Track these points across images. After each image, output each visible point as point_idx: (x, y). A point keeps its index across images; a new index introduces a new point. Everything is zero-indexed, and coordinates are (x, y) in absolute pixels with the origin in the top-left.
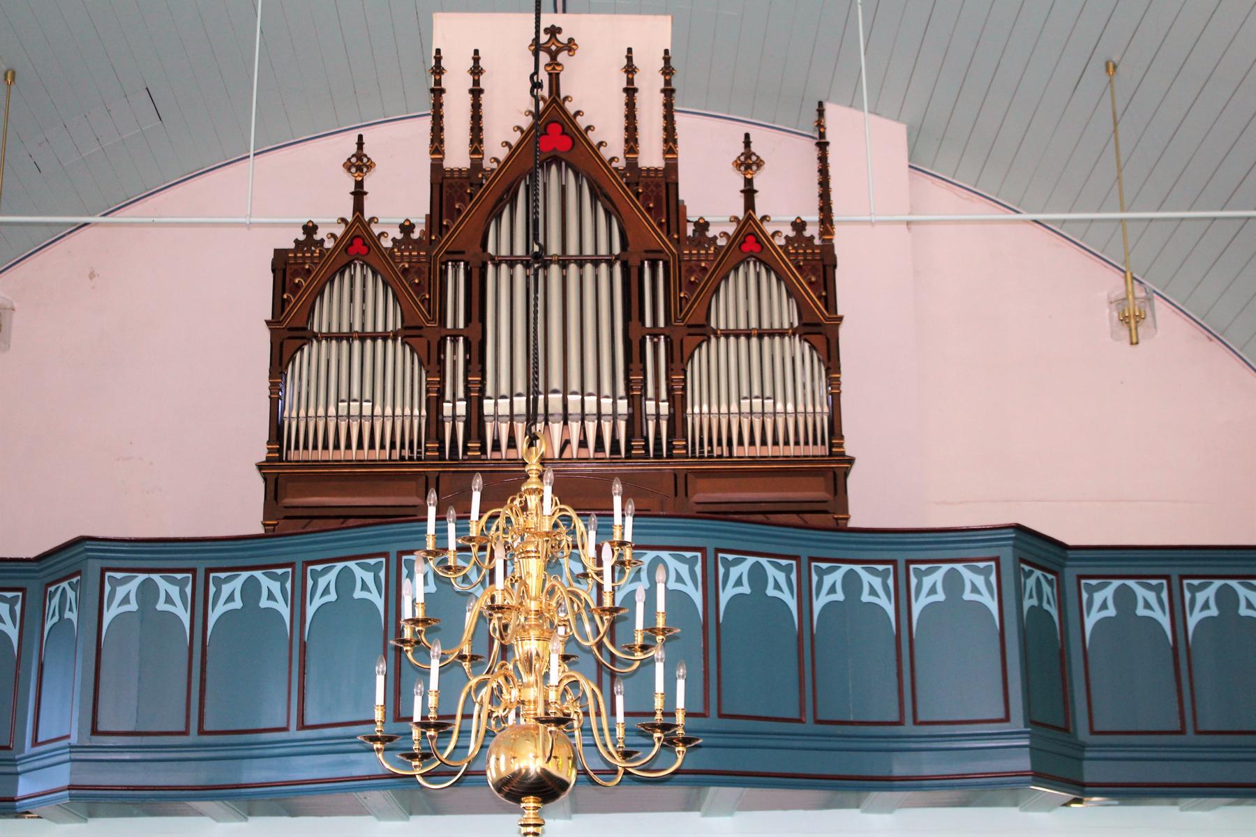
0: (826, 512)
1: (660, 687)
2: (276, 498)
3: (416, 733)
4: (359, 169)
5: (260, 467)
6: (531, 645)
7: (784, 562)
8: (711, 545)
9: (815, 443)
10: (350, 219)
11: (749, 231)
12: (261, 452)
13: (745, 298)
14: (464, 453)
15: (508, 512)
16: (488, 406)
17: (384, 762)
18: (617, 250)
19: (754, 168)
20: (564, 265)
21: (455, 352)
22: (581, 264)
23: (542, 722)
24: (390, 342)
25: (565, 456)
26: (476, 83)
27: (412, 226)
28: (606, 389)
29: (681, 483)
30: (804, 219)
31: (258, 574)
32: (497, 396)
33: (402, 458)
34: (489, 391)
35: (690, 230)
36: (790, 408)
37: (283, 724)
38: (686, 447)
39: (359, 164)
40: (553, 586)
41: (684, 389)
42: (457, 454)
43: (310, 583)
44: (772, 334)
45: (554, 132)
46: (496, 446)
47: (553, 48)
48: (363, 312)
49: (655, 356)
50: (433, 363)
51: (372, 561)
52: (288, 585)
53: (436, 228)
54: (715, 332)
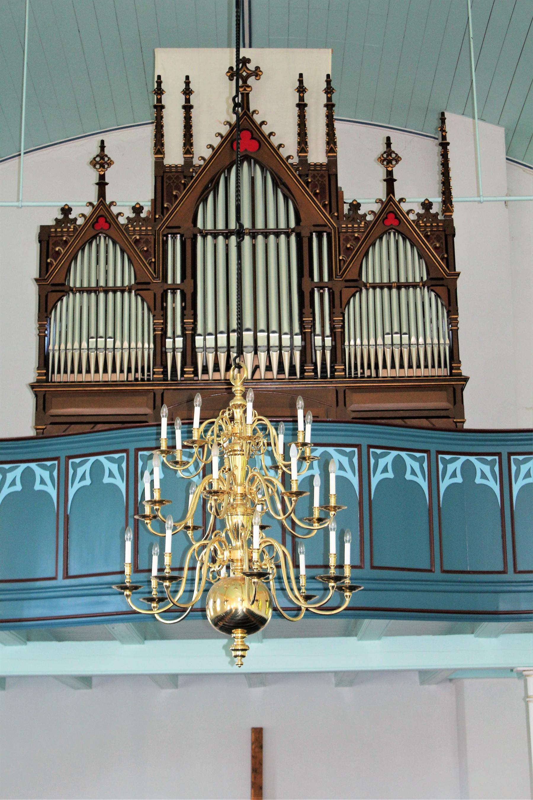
0: (448, 417)
1: (333, 549)
2: (44, 409)
3: (154, 583)
4: (102, 166)
5: (32, 387)
6: (238, 519)
7: (418, 455)
8: (364, 442)
9: (440, 366)
10: (95, 203)
11: (391, 209)
12: (32, 376)
13: (389, 259)
14: (182, 375)
15: (220, 422)
16: (199, 341)
17: (131, 602)
18: (292, 225)
19: (394, 162)
20: (254, 237)
21: (174, 301)
22: (266, 235)
23: (248, 575)
24: (126, 294)
25: (255, 377)
26: (188, 100)
27: (141, 208)
28: (286, 328)
29: (341, 398)
30: (430, 200)
31: (33, 466)
32: (206, 334)
33: (136, 380)
34: (200, 330)
35: (346, 207)
36: (421, 340)
37: (53, 575)
38: (344, 370)
39: (102, 161)
40: (254, 476)
41: (343, 327)
42: (177, 376)
43: (71, 471)
44: (407, 286)
45: (245, 139)
46: (205, 370)
47: (244, 74)
48: (106, 272)
49: (321, 303)
50: (158, 309)
51: (116, 456)
52: (55, 473)
53: (159, 209)
54: (365, 285)
